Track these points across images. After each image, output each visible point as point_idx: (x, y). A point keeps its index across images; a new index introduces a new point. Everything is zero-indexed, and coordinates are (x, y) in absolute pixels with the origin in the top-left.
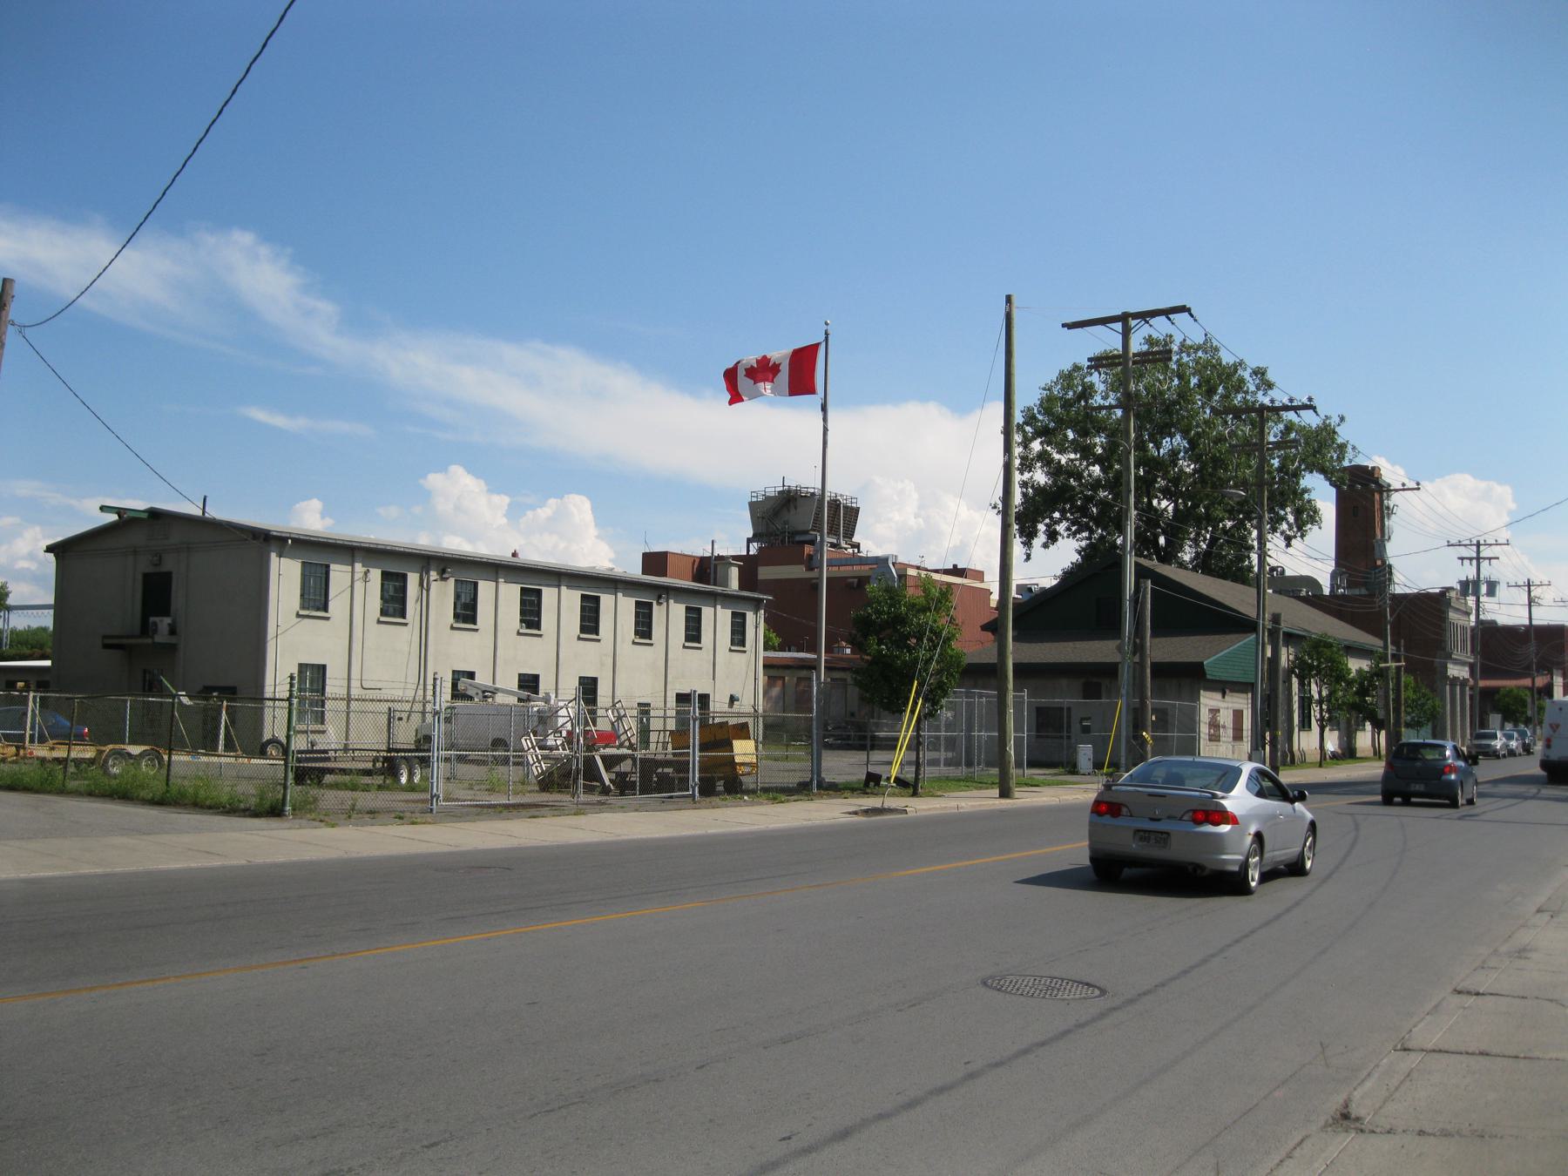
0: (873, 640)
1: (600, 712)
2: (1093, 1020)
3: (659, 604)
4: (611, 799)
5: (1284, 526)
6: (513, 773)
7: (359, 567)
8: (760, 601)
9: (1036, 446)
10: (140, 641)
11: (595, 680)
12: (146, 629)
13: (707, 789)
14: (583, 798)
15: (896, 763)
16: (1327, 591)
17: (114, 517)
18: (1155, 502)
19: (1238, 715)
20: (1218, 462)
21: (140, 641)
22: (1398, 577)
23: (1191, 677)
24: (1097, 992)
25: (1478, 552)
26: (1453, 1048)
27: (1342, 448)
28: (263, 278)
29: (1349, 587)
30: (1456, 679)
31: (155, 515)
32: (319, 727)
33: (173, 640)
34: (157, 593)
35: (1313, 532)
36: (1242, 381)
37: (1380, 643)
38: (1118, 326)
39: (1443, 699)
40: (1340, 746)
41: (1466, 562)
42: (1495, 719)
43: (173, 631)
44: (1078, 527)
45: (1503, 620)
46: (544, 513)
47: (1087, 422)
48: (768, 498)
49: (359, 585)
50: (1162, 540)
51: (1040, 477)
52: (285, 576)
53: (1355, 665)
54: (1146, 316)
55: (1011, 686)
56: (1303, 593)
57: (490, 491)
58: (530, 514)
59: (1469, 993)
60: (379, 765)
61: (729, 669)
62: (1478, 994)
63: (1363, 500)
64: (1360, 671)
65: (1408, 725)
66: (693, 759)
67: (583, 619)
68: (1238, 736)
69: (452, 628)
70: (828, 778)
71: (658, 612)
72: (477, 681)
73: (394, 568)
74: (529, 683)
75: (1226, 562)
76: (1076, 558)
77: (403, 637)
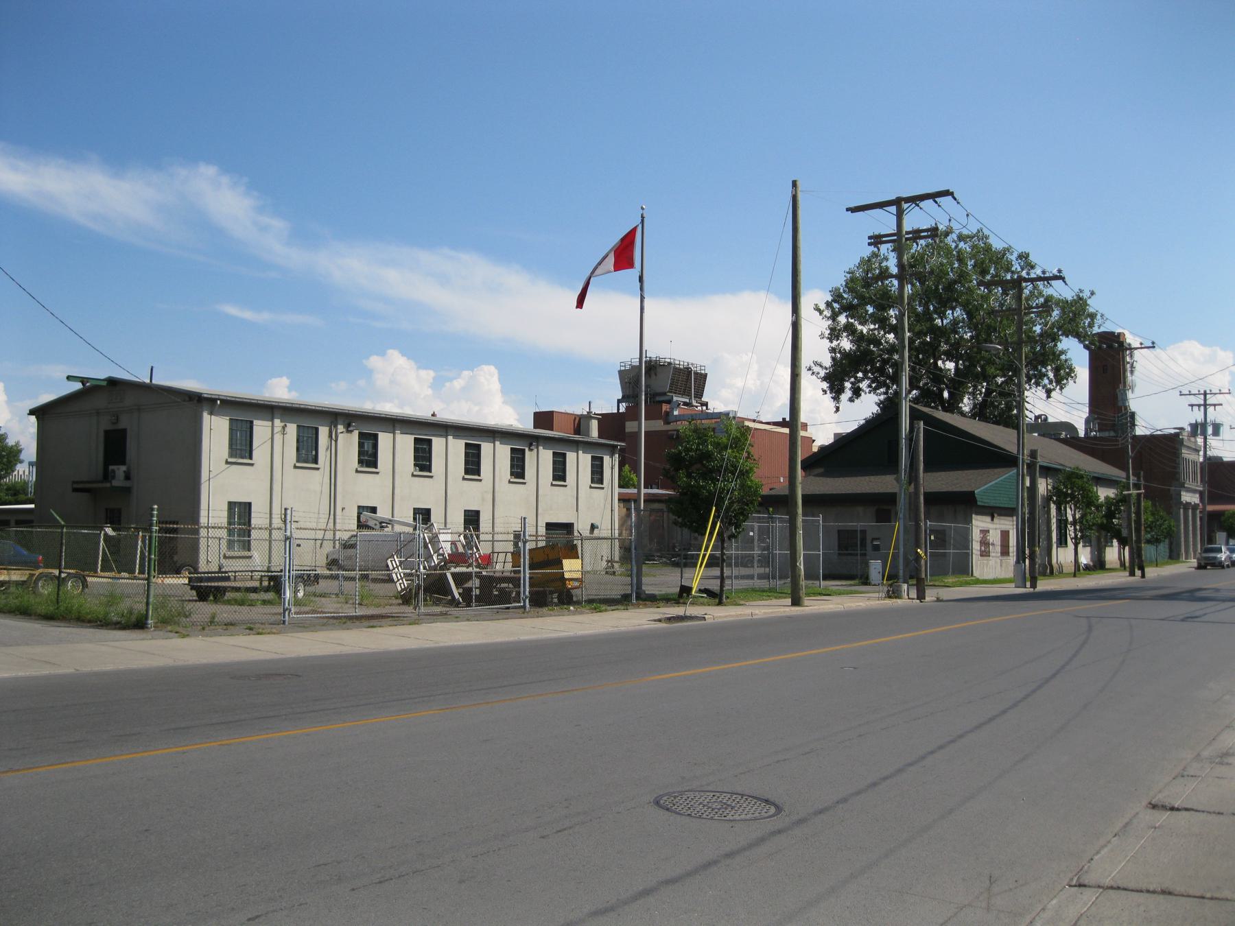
0: (682, 473)
1: (482, 537)
2: (750, 846)
3: (531, 450)
4: (453, 611)
5: (1046, 381)
6: (379, 588)
7: (277, 422)
8: (615, 447)
9: (842, 319)
10: (100, 485)
11: (477, 513)
12: (107, 476)
13: (539, 600)
14: (423, 610)
15: (697, 578)
16: (1082, 434)
17: (78, 386)
18: (940, 363)
19: (1005, 535)
20: (990, 329)
21: (100, 485)
22: (1138, 421)
23: (966, 504)
24: (773, 810)
25: (1205, 400)
26: (1132, 885)
27: (1092, 316)
28: (226, 201)
29: (1100, 430)
30: (1188, 504)
31: (113, 383)
32: (247, 553)
33: (127, 484)
34: (115, 446)
35: (1070, 386)
36: (1010, 264)
37: (1123, 474)
38: (893, 209)
39: (1178, 520)
40: (1092, 559)
41: (1196, 408)
42: (1221, 536)
43: (128, 477)
44: (876, 386)
46: (458, 384)
47: (884, 301)
49: (278, 437)
50: (946, 394)
51: (846, 344)
52: (215, 432)
53: (1104, 493)
54: (916, 200)
55: (800, 511)
56: (1063, 436)
57: (419, 368)
58: (448, 384)
59: (1164, 807)
60: (265, 583)
61: (592, 504)
62: (1172, 809)
63: (1110, 359)
64: (1107, 498)
65: (1148, 542)
66: (542, 576)
67: (466, 463)
68: (1005, 552)
69: (357, 471)
70: (648, 589)
71: (529, 457)
72: (378, 515)
73: (367, 430)
74: (424, 515)
75: (1002, 408)
76: (876, 409)
77: (316, 480)
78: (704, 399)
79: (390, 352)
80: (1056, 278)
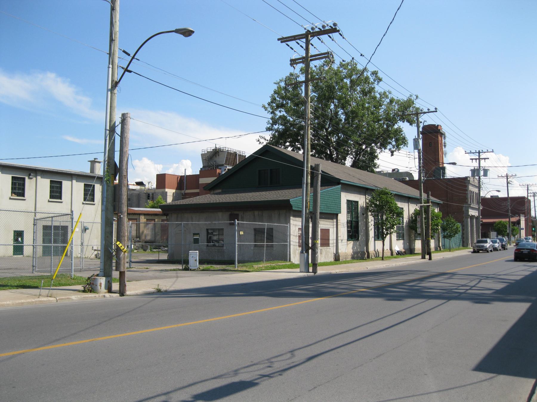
3: (29, 178)
25: (479, 156)
30: (472, 216)
36: (367, 78)
41: (474, 161)
63: (432, 138)
79: (144, 158)
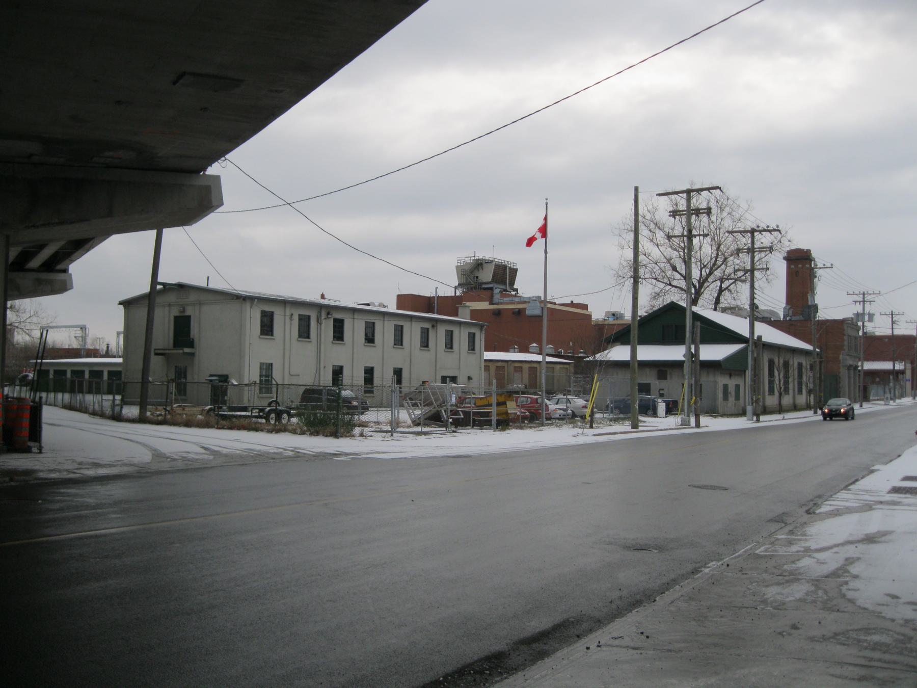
16: (782, 318)
34: (182, 326)
38: (685, 195)
45: (879, 332)
48: (467, 264)
54: (699, 191)
63: (801, 266)
77: (308, 349)
78: (515, 287)
80: (775, 230)
